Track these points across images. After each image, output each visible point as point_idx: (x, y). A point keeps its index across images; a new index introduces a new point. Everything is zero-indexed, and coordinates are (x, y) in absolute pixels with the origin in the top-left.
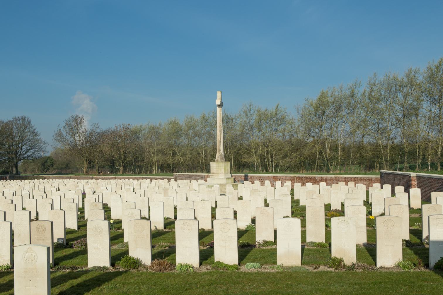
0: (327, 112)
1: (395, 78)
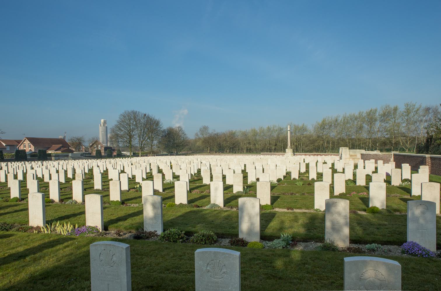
0: (326, 127)
1: (354, 115)
